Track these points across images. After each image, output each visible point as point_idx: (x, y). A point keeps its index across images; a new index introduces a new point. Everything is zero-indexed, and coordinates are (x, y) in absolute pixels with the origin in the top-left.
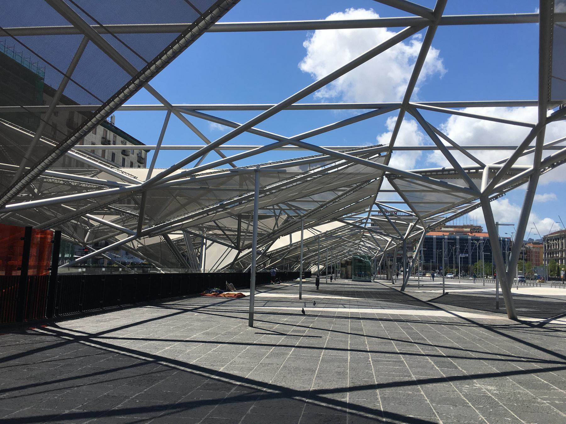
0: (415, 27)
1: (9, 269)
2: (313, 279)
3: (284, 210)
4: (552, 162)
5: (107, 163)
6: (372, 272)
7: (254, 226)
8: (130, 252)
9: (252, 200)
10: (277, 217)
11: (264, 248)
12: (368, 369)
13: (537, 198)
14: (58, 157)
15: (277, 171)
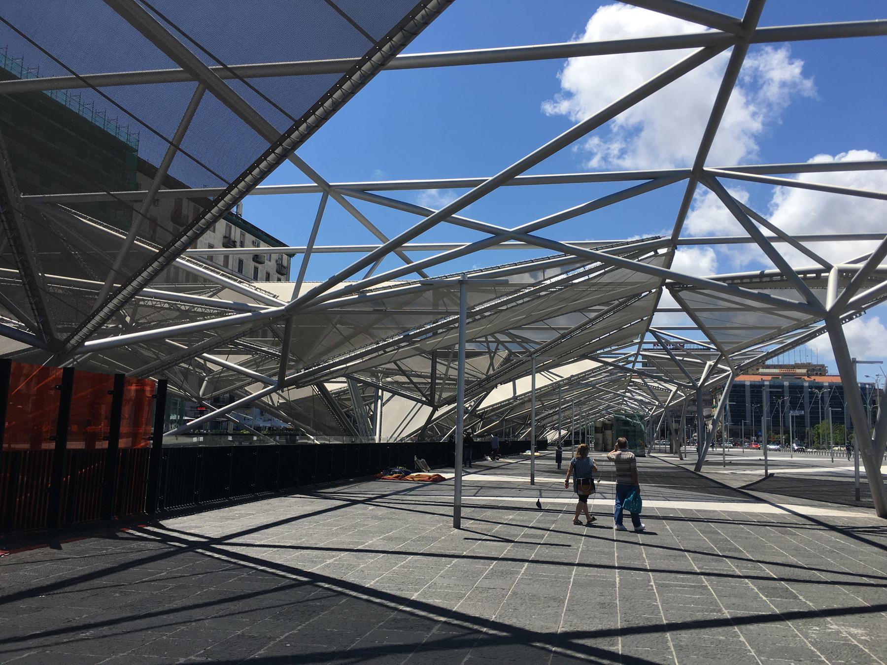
0: (710, 47)
1: (91, 439)
3: (502, 343)
5: (232, 275)
6: (646, 442)
7: (460, 369)
8: (266, 410)
9: (453, 328)
10: (492, 354)
11: (472, 404)
12: (650, 599)
15: (492, 282)
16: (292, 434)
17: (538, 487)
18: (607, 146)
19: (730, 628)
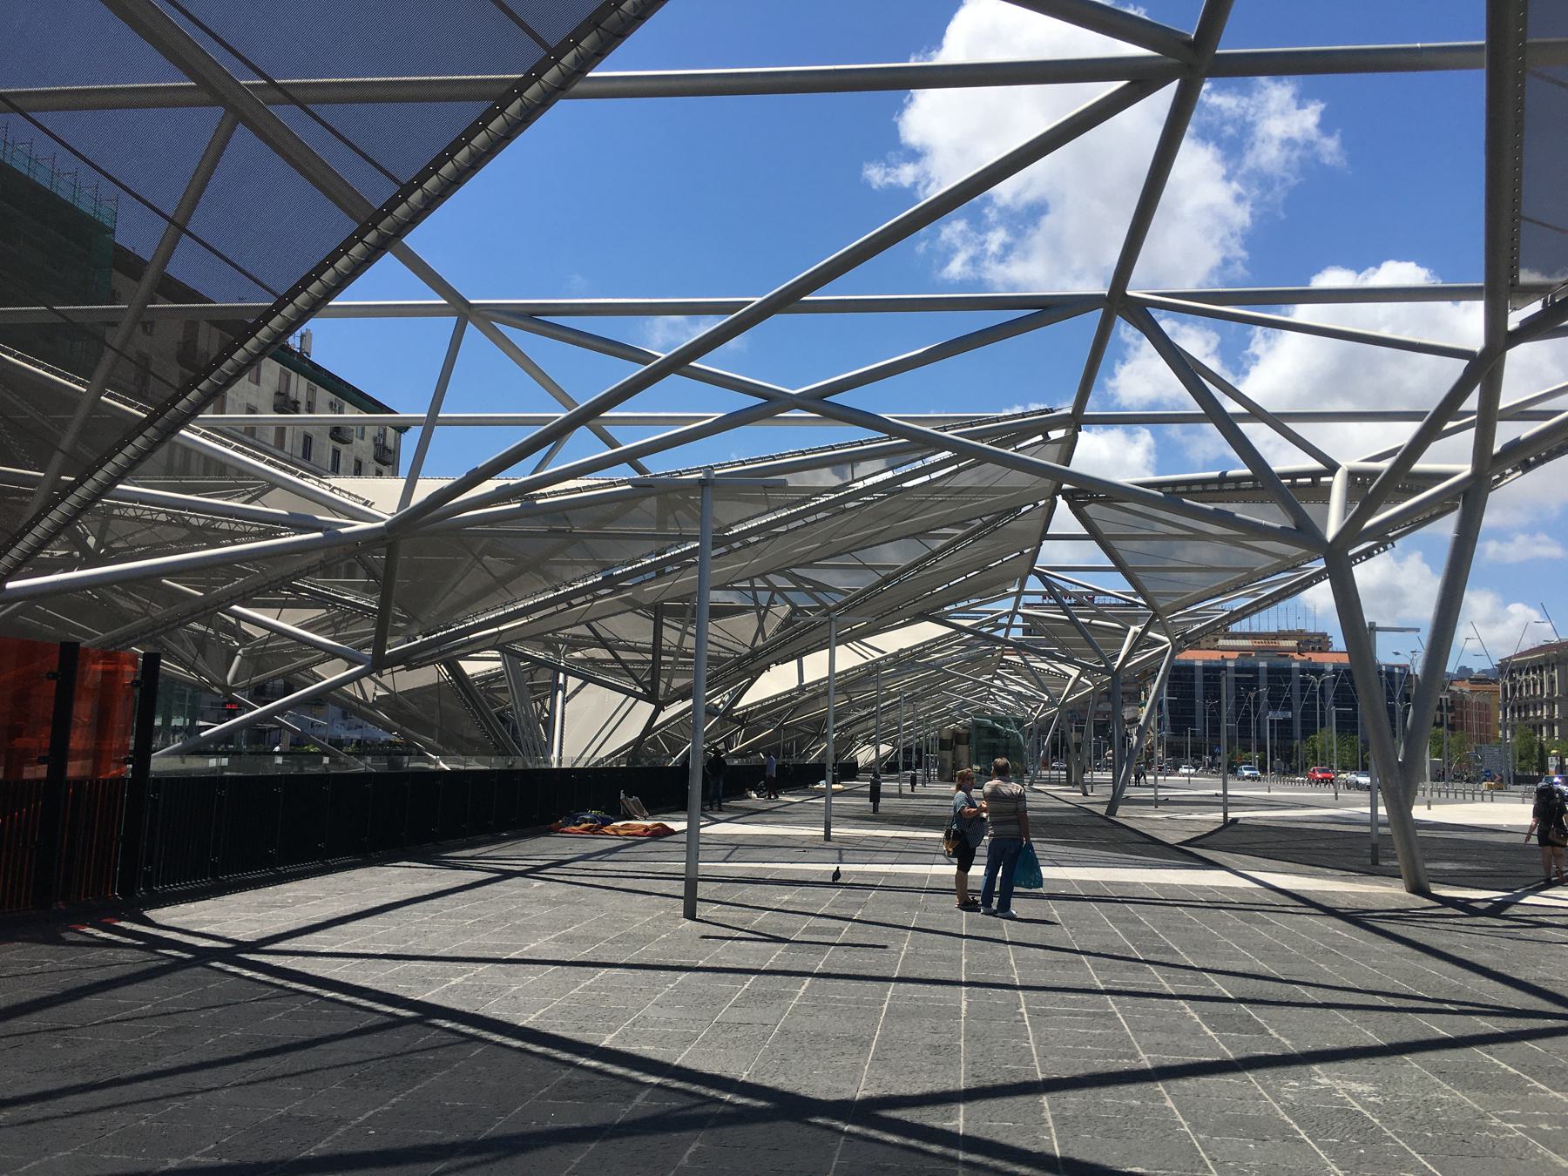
0: (1138, 81)
2: (863, 785)
3: (781, 591)
4: (1524, 456)
5: (290, 462)
8: (352, 710)
9: (691, 564)
10: (762, 612)
11: (726, 698)
13: (1486, 550)
14: (152, 447)
15: (761, 483)
16: (390, 751)
17: (837, 845)
18: (982, 238)
19: (1151, 1085)
